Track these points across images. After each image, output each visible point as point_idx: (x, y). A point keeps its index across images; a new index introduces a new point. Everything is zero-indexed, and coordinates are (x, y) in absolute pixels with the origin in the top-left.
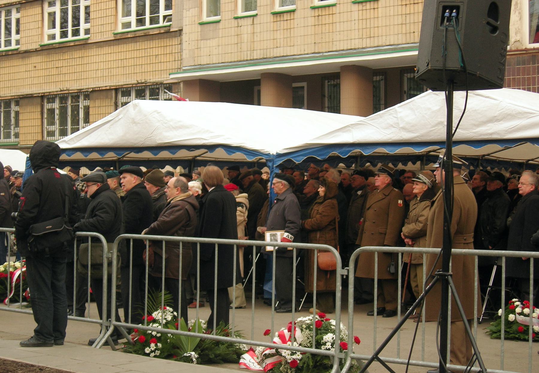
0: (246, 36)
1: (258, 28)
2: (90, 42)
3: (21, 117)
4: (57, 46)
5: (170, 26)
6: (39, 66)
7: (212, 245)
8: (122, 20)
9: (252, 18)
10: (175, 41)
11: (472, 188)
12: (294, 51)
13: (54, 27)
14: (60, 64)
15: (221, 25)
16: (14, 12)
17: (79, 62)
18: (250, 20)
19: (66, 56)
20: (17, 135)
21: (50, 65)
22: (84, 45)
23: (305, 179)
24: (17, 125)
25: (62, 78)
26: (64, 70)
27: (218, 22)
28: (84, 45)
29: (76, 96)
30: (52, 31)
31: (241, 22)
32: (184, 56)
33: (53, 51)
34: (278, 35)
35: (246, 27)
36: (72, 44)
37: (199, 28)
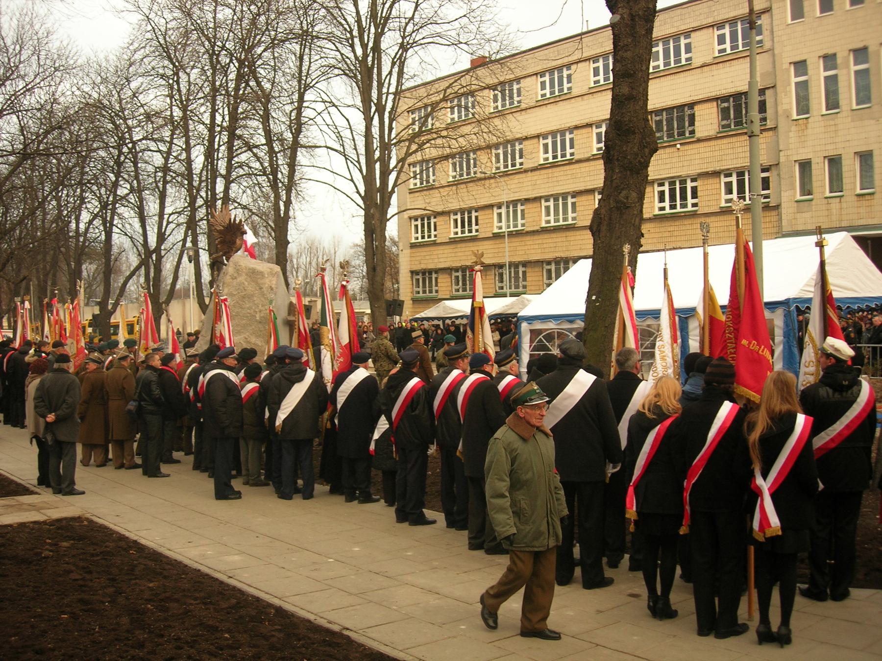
0: (834, 211)
1: (844, 205)
2: (698, 213)
3: (439, 280)
4: (669, 216)
5: (768, 202)
6: (652, 230)
7: (877, 347)
8: (544, 218)
9: (839, 199)
10: (774, 213)
11: (843, 338)
12: (871, 222)
13: (457, 227)
14: (672, 229)
15: (813, 202)
16: (519, 205)
17: (688, 227)
18: (838, 200)
19: (677, 223)
20: (437, 291)
21: (662, 230)
22: (434, 244)
23: (27, 359)
24: (436, 285)
25: (673, 239)
26: (676, 233)
27: (811, 200)
28: (434, 244)
29: (430, 272)
30: (456, 230)
31: (830, 200)
32: (783, 224)
33: (665, 219)
34: (862, 210)
35: (834, 205)
36: (683, 214)
37: (796, 204)
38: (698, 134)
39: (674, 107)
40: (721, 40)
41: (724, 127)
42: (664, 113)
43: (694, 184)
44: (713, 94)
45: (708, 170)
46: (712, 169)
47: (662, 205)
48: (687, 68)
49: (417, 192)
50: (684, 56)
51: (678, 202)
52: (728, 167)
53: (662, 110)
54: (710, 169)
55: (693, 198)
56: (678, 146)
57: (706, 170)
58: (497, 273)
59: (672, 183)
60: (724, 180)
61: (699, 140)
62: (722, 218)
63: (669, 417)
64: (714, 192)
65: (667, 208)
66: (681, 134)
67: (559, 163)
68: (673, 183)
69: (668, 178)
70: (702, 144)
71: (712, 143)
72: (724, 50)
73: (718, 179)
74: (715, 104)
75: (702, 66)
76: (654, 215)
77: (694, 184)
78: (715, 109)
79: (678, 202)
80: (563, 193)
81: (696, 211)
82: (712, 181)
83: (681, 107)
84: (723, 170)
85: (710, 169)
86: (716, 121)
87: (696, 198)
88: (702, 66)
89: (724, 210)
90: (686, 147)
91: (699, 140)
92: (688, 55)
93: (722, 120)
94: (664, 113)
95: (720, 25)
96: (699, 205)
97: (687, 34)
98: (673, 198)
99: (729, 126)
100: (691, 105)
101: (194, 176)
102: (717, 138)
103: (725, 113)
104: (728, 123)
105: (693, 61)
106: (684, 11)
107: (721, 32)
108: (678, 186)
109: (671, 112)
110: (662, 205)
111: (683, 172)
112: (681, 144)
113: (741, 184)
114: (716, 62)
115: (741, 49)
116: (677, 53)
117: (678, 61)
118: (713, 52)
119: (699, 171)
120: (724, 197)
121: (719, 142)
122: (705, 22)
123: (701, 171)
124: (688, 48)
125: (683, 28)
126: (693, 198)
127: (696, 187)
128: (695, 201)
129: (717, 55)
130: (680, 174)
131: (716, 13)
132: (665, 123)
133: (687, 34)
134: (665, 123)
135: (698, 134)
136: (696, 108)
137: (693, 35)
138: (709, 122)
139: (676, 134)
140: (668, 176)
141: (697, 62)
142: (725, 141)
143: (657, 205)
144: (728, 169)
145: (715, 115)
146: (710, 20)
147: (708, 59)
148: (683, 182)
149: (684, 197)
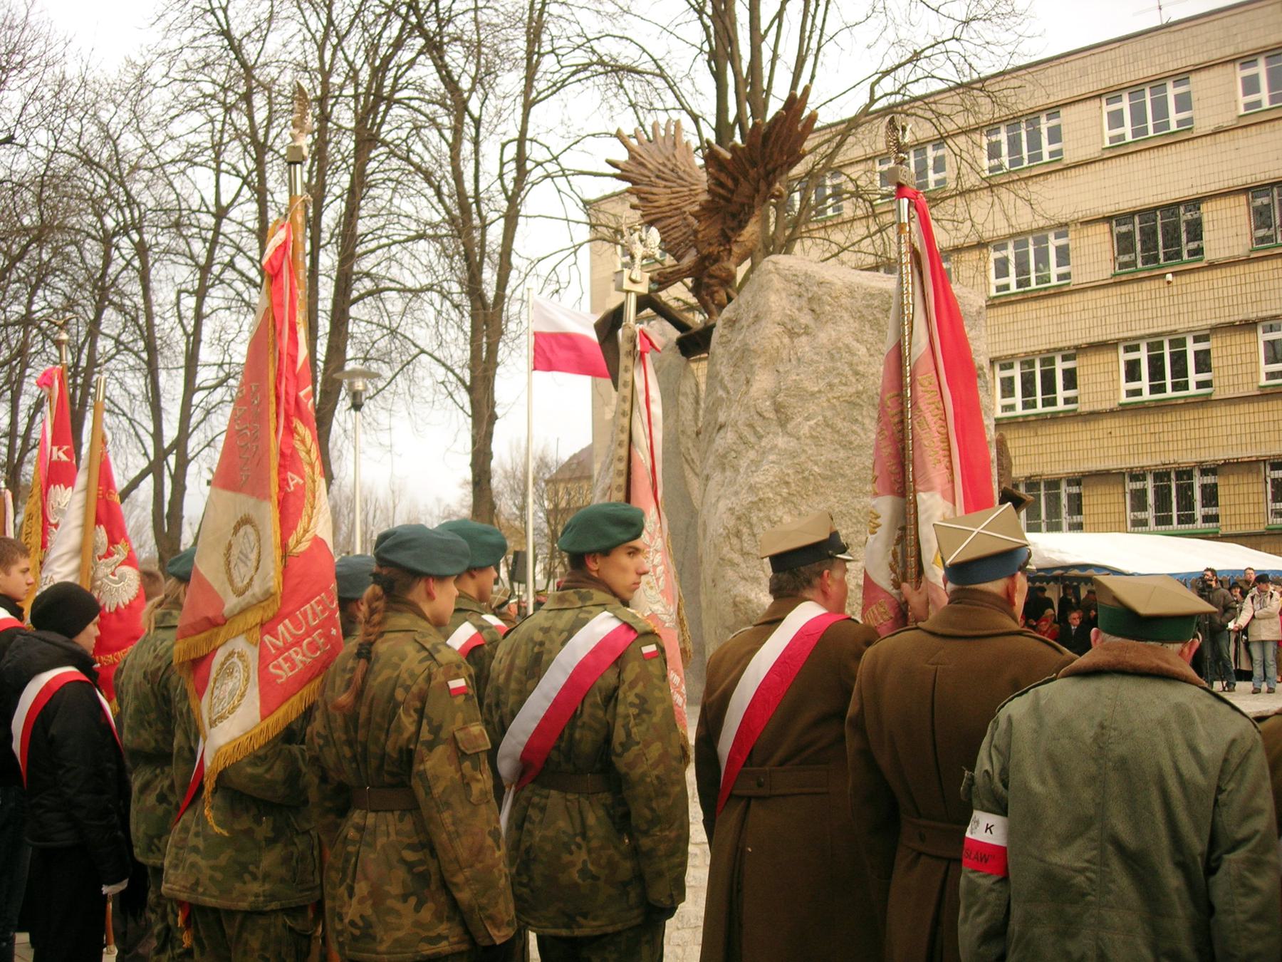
2: (1214, 397)
4: (1153, 404)
6: (1116, 432)
38: (1209, 256)
39: (1156, 208)
40: (1116, 119)
41: (1262, 240)
42: (1137, 219)
43: (1202, 346)
44: (1239, 182)
45: (1232, 319)
46: (1241, 318)
47: (1008, 401)
48: (1186, 135)
49: (1012, 303)
50: (1046, 148)
51: (1039, 397)
52: (1274, 313)
53: (1133, 214)
54: (1236, 318)
55: (1066, 388)
56: (1169, 277)
57: (1227, 320)
58: (1269, 480)
59: (1155, 346)
60: (1124, 357)
61: (1212, 266)
62: (1263, 406)
63: (782, 763)
64: (1246, 359)
65: (1146, 391)
66: (1174, 255)
67: (1013, 298)
68: (1031, 364)
69: (1171, 333)
70: (1218, 273)
71: (1239, 270)
72: (1122, 137)
73: (1114, 355)
74: (1243, 199)
75: (1215, 133)
76: (1120, 405)
77: (1202, 346)
78: (1244, 209)
79: (1039, 397)
80: (1150, 336)
81: (1211, 394)
82: (1239, 339)
83: (1171, 208)
84: (1264, 319)
85: (1237, 317)
86: (1246, 230)
87: (1075, 387)
88: (1215, 133)
89: (1268, 391)
90: (1186, 279)
91: (1212, 266)
92: (1055, 147)
93: (1257, 228)
94: (1137, 219)
95: (1112, 94)
96: (1215, 383)
97: (1181, 77)
98: (1028, 390)
99: (1134, 263)
100: (1195, 203)
101: (320, 313)
102: (1249, 261)
103: (1124, 244)
104: (1269, 233)
105: (1196, 124)
106: (1173, 37)
107: (1249, 72)
108: (1038, 370)
109: (1152, 216)
110: (1008, 401)
111: (1180, 324)
112: (1174, 274)
113: (1028, 382)
114: (1242, 125)
115: (1151, 133)
116: (1035, 143)
117: (1161, 126)
118: (1236, 109)
119: (1214, 322)
120: (1125, 386)
121: (1254, 267)
122: (1216, 55)
123: (1218, 321)
124: (1055, 135)
125: (1172, 66)
126: (1066, 388)
127: (1207, 352)
128: (1204, 377)
129: (1242, 112)
130: (1173, 328)
131: (1239, 38)
132: (1138, 237)
133: (1053, 110)
134: (1138, 237)
135: (1209, 256)
136: (1204, 207)
137: (1063, 112)
138: (1232, 232)
139: (1161, 256)
140: (1147, 332)
141: (1201, 126)
142: (1265, 265)
143: (999, 401)
144: (1006, 357)
145: (1108, 246)
146: (1229, 51)
147: (1227, 120)
148: (1178, 343)
149: (1049, 386)
